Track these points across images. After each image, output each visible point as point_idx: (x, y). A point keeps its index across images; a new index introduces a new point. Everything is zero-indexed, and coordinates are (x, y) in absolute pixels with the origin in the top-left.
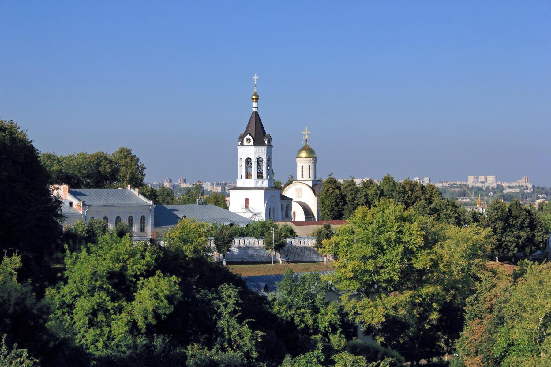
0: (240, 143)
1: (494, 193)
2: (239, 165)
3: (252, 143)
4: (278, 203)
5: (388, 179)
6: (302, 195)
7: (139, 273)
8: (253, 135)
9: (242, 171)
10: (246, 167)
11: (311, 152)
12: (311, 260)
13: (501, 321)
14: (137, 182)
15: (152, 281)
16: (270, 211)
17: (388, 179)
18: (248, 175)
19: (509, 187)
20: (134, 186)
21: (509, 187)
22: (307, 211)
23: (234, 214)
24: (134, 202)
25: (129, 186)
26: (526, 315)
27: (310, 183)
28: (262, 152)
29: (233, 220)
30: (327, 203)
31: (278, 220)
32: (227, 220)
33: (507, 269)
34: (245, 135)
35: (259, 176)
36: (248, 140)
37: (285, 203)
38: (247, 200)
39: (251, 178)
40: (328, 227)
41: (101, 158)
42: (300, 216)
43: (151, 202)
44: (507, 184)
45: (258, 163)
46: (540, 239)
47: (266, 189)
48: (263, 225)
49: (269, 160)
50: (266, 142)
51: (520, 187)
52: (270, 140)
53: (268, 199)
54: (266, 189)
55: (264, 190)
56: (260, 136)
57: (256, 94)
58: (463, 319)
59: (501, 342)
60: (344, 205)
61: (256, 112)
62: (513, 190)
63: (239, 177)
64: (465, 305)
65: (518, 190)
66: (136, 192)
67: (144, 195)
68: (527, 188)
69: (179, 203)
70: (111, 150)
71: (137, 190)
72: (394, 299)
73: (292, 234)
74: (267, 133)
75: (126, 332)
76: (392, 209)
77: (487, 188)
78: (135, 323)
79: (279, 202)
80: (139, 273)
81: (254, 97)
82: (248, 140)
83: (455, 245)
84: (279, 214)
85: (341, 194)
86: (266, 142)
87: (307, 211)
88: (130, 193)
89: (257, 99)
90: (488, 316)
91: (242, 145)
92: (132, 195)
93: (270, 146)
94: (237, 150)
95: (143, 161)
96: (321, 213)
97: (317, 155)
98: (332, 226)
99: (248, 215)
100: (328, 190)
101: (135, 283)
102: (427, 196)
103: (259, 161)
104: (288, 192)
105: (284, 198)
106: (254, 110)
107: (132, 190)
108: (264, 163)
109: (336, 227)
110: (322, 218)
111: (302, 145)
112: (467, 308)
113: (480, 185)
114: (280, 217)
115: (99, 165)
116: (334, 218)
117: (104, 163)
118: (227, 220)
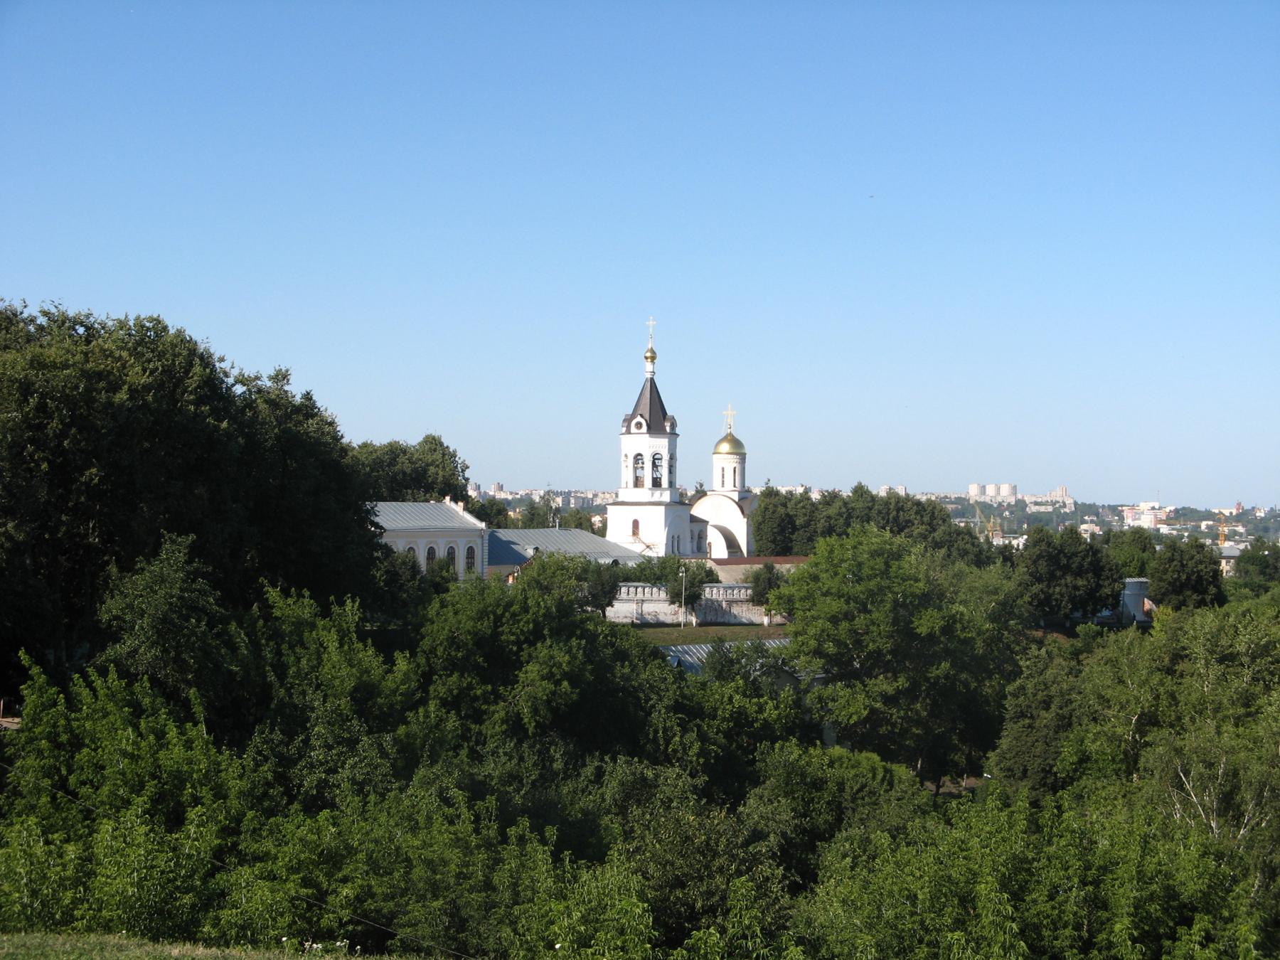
0: (624, 430)
1: (1011, 513)
2: (623, 465)
3: (644, 428)
4: (687, 529)
5: (860, 491)
6: (724, 516)
7: (522, 638)
8: (647, 416)
9: (628, 475)
10: (635, 469)
11: (737, 446)
12: (720, 620)
13: (1065, 724)
14: (459, 494)
15: (542, 650)
16: (673, 541)
17: (860, 491)
18: (638, 482)
19: (1036, 504)
20: (455, 499)
21: (1036, 504)
22: (731, 543)
23: (616, 546)
24: (456, 525)
25: (448, 498)
26: (1110, 713)
27: (736, 496)
28: (661, 445)
29: (616, 554)
30: (765, 528)
31: (687, 556)
32: (607, 555)
33: (1057, 640)
34: (633, 416)
35: (656, 483)
36: (639, 425)
37: (696, 527)
38: (636, 524)
39: (643, 486)
40: (770, 568)
41: (395, 451)
42: (719, 549)
43: (483, 525)
44: (1033, 499)
45: (654, 463)
46: (1107, 591)
47: (667, 505)
48: (663, 562)
49: (672, 457)
50: (668, 429)
51: (1053, 503)
52: (673, 426)
53: (670, 522)
54: (667, 505)
55: (662, 508)
56: (656, 416)
57: (652, 351)
58: (1002, 720)
59: (1068, 753)
60: (793, 533)
61: (652, 380)
62: (1042, 509)
63: (623, 485)
64: (1005, 697)
65: (1050, 509)
66: (459, 508)
67: (471, 512)
68: (1064, 505)
69: (514, 525)
70: (412, 438)
71: (461, 504)
72: (882, 684)
73: (712, 578)
74: (669, 412)
75: (503, 733)
76: (876, 536)
77: (1000, 504)
78: (518, 717)
79: (687, 526)
80: (522, 638)
81: (648, 354)
82: (639, 425)
83: (974, 599)
84: (687, 546)
85: (787, 515)
86: (668, 429)
87: (731, 543)
88: (449, 510)
89: (653, 358)
90: (1043, 713)
91: (628, 432)
92: (454, 515)
93: (673, 435)
94: (620, 441)
95: (462, 456)
96: (754, 547)
97: (747, 450)
98: (777, 566)
99: (637, 548)
100: (766, 509)
101: (517, 653)
102: (926, 519)
103: (655, 461)
104: (699, 510)
105: (694, 519)
106: (649, 376)
107: (453, 505)
108: (664, 464)
109: (785, 567)
110: (755, 553)
111: (723, 435)
112: (1009, 703)
113: (987, 500)
114: (688, 551)
115: (393, 462)
116: (778, 554)
117: (402, 459)
118: (607, 555)
